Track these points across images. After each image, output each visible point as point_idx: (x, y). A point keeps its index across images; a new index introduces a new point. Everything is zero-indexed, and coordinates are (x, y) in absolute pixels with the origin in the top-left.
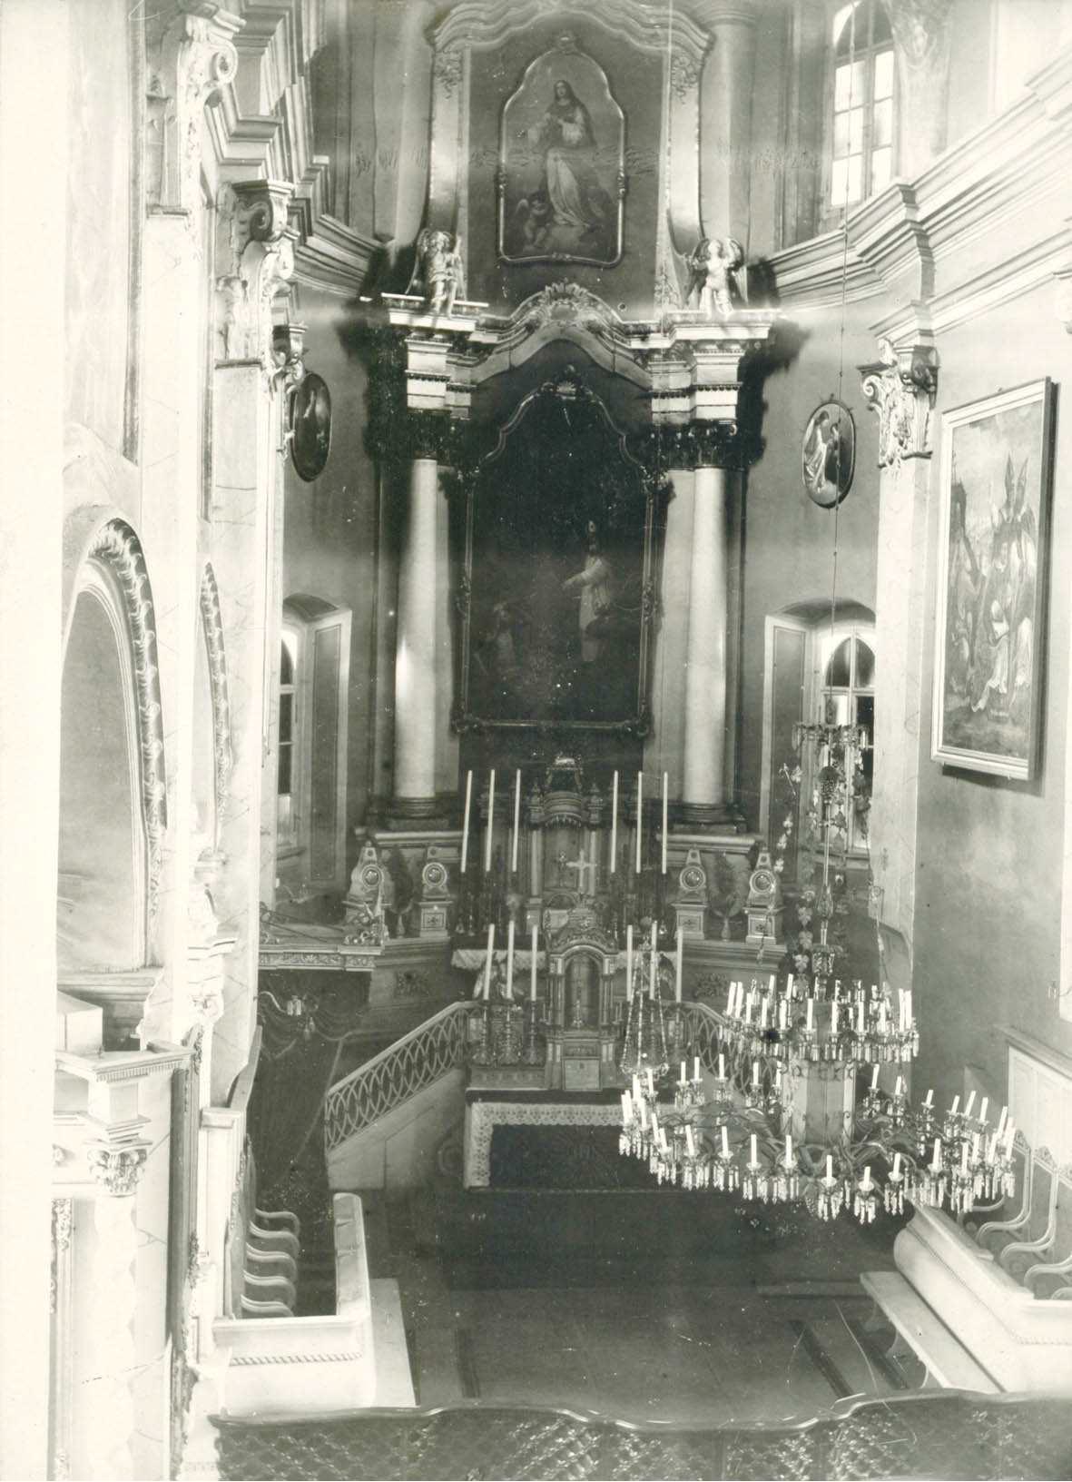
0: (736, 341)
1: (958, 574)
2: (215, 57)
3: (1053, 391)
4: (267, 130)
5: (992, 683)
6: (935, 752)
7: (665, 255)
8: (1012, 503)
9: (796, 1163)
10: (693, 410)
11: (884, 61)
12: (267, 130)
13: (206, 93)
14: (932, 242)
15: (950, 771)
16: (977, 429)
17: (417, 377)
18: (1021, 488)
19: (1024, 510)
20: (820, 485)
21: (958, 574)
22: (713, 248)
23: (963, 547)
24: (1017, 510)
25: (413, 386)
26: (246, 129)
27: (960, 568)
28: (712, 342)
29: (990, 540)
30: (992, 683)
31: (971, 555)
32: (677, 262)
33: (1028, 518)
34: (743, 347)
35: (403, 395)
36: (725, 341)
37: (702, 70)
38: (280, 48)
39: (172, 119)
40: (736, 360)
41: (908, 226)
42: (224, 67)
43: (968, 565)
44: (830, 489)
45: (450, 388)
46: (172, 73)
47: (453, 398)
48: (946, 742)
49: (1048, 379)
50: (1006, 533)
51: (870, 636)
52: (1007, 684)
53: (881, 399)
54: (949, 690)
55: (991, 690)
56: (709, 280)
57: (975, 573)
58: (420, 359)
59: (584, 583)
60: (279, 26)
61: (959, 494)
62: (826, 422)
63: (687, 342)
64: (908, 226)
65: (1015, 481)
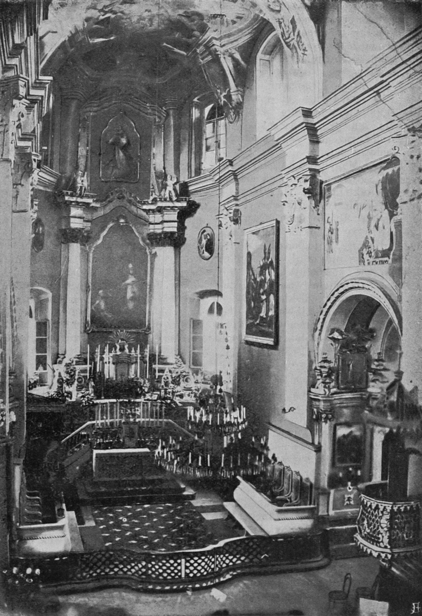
0: (176, 207)
1: (250, 280)
2: (20, 113)
3: (278, 222)
4: (31, 137)
5: (261, 315)
6: (243, 338)
7: (153, 180)
8: (266, 257)
9: (92, 605)
10: (163, 228)
11: (222, 123)
12: (31, 137)
13: (17, 123)
14: (239, 177)
15: (248, 343)
16: (254, 235)
17: (75, 217)
18: (269, 253)
19: (270, 260)
20: (203, 253)
21: (250, 280)
22: (169, 178)
23: (251, 271)
24: (268, 259)
25: (72, 220)
26: (24, 137)
27: (250, 279)
28: (169, 207)
29: (259, 269)
30: (261, 315)
31: (253, 274)
32: (157, 182)
33: (271, 262)
34: (179, 209)
35: (69, 223)
36: (173, 207)
37: (17, 195)
38: (36, 113)
39: (7, 131)
40: (177, 213)
41: (304, 125)
42: (23, 116)
43: (253, 277)
44: (207, 254)
45: (84, 221)
46: (8, 117)
47: (86, 224)
48: (247, 334)
49: (276, 219)
50: (263, 268)
51: (220, 300)
52: (266, 315)
53: (223, 225)
54: (247, 318)
55: (261, 317)
56: (168, 188)
57: (255, 279)
58: (75, 211)
59: (128, 284)
60: (36, 106)
61: (249, 255)
62: (205, 233)
63: (161, 207)
64: (304, 125)
65: (267, 251)
